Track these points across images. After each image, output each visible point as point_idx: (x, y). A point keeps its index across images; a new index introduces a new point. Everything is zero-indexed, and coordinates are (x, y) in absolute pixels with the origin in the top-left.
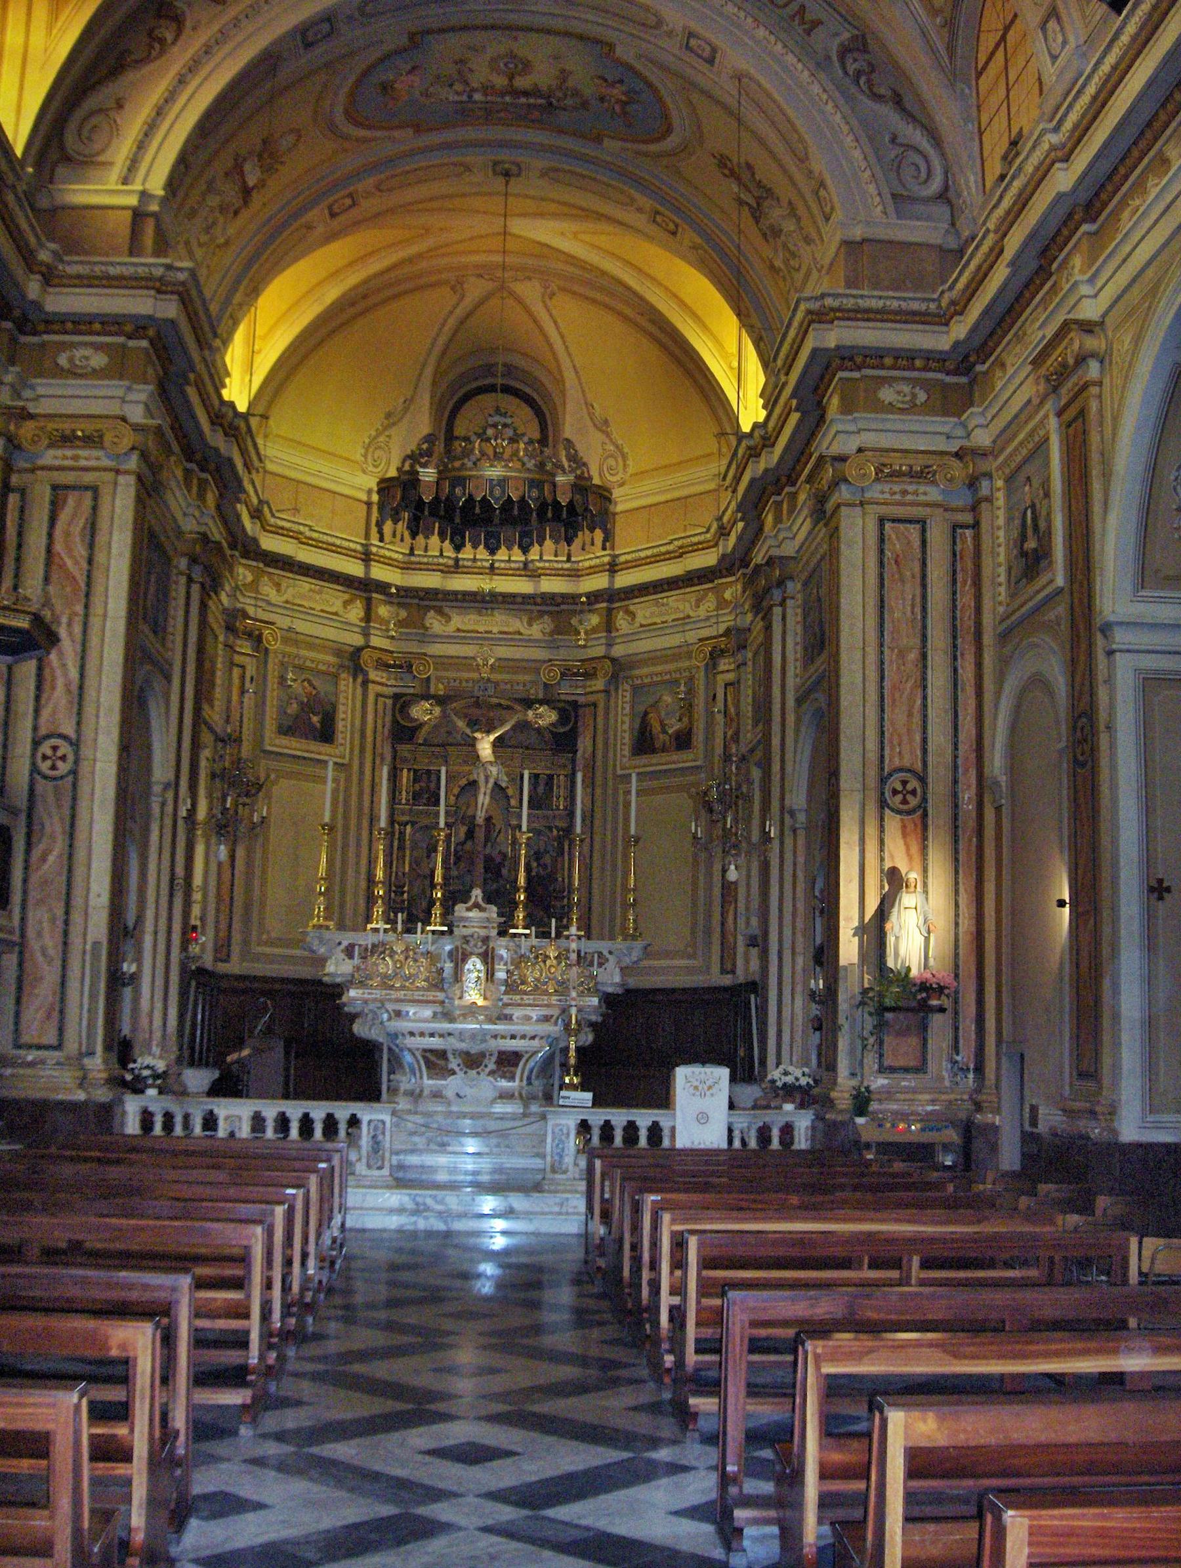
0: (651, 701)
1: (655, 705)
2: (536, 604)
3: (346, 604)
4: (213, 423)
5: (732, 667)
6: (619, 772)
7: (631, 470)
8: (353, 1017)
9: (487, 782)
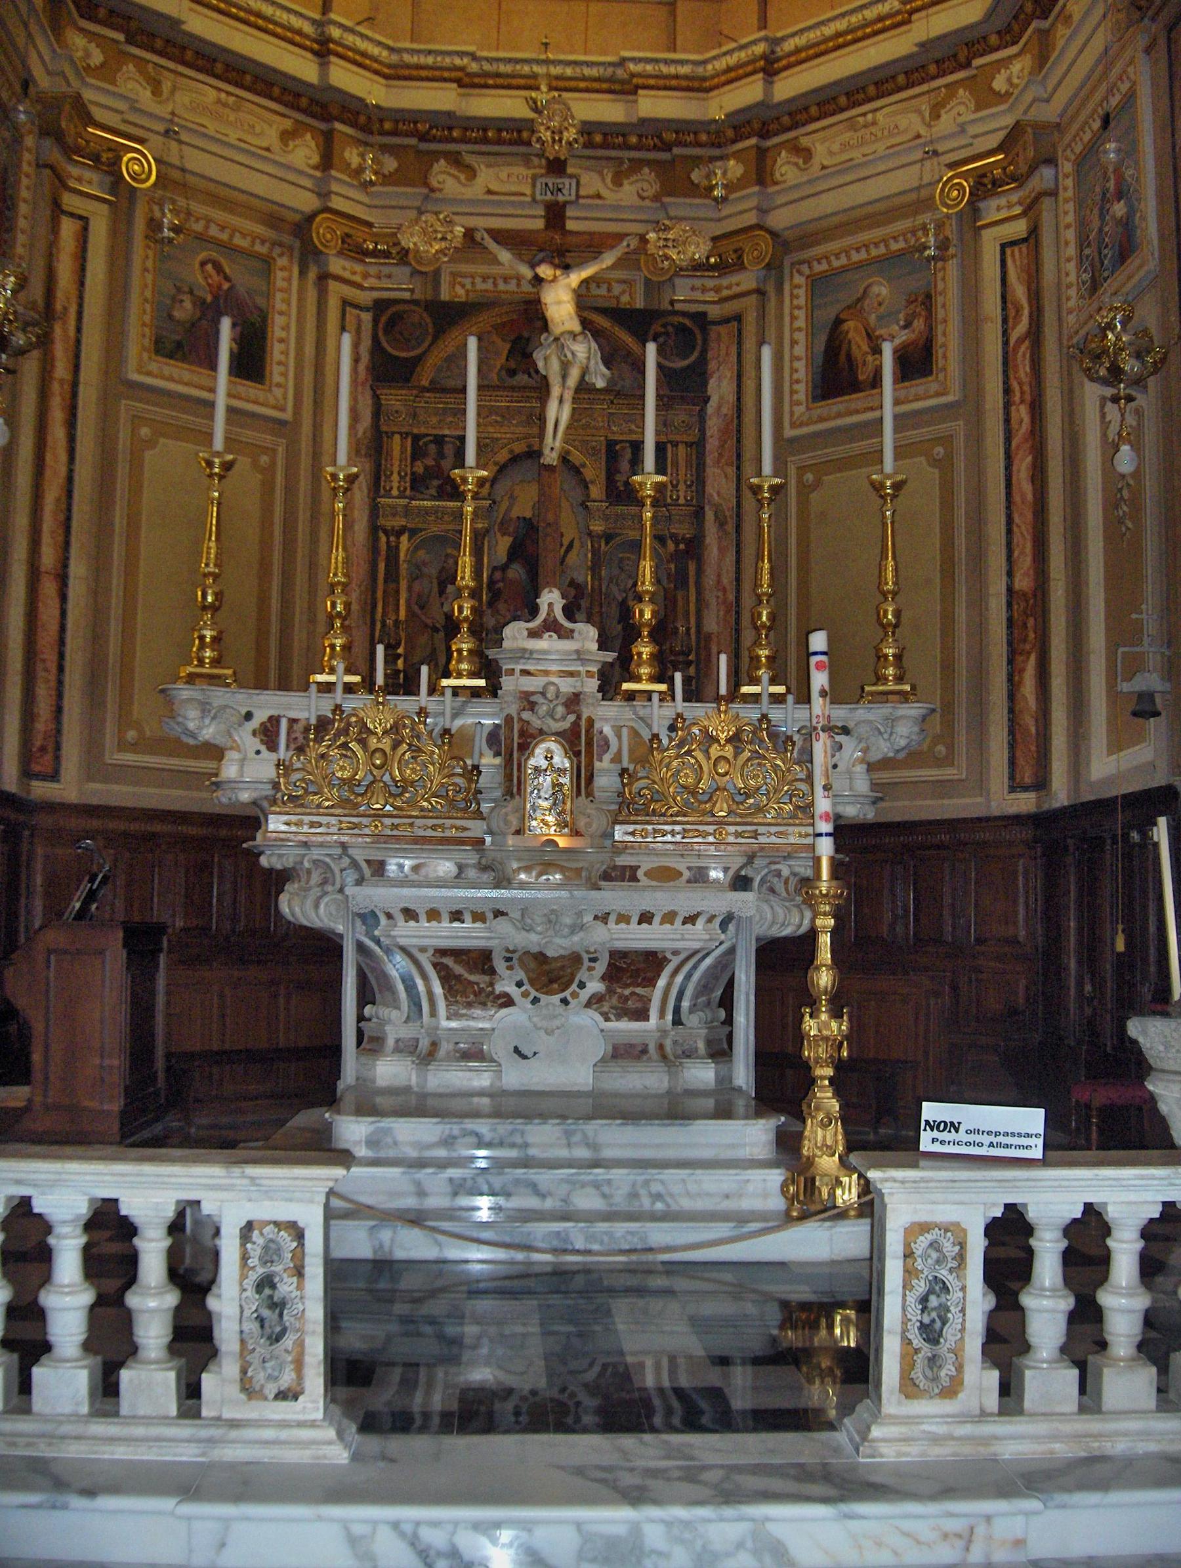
2: (626, 146)
3: (286, 136)
5: (1018, 210)
6: (789, 433)
8: (279, 879)
9: (564, 377)
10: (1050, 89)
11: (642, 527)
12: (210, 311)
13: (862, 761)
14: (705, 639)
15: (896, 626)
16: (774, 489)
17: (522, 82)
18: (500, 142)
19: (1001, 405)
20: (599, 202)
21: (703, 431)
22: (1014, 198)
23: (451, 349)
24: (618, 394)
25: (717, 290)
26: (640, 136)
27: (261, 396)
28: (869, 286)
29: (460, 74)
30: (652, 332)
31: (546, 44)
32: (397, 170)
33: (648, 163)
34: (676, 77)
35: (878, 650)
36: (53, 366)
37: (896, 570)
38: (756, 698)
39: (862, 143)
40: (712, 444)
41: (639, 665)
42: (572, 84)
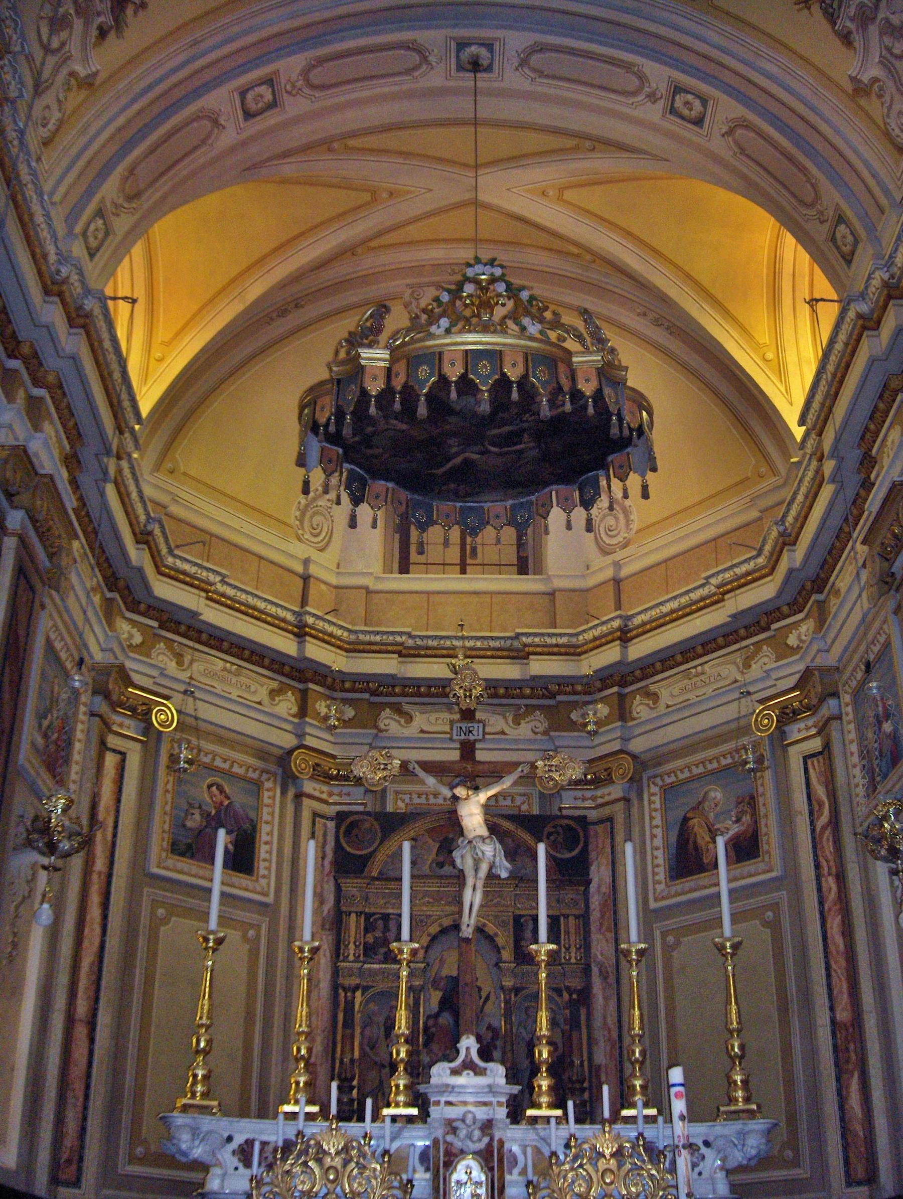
0: (693, 802)
1: (698, 807)
2: (522, 696)
3: (273, 693)
4: (47, 292)
5: (813, 731)
6: (653, 905)
7: (635, 526)
9: (476, 870)
10: (829, 641)
11: (538, 983)
12: (214, 821)
13: (722, 1168)
14: (595, 1070)
15: (741, 1057)
16: (641, 953)
17: (445, 652)
18: (429, 695)
19: (814, 877)
20: (503, 737)
21: (587, 906)
22: (810, 723)
23: (394, 849)
24: (521, 879)
25: (593, 798)
26: (532, 688)
27: (250, 884)
28: (706, 793)
29: (400, 648)
30: (545, 833)
31: (462, 625)
32: (354, 717)
33: (540, 707)
34: (557, 645)
35: (728, 1077)
36: (94, 862)
37: (739, 1012)
38: (632, 1120)
39: (695, 687)
40: (595, 915)
41: (539, 1095)
42: (482, 653)
